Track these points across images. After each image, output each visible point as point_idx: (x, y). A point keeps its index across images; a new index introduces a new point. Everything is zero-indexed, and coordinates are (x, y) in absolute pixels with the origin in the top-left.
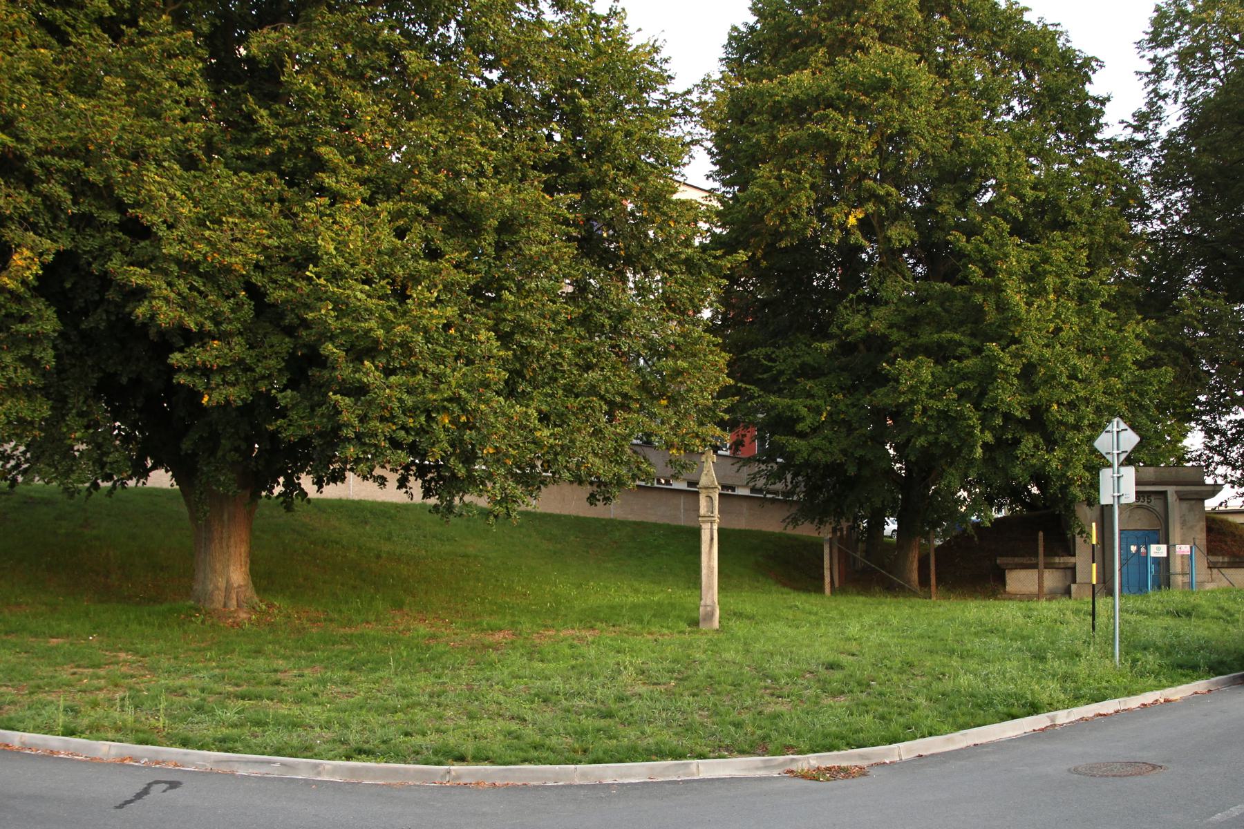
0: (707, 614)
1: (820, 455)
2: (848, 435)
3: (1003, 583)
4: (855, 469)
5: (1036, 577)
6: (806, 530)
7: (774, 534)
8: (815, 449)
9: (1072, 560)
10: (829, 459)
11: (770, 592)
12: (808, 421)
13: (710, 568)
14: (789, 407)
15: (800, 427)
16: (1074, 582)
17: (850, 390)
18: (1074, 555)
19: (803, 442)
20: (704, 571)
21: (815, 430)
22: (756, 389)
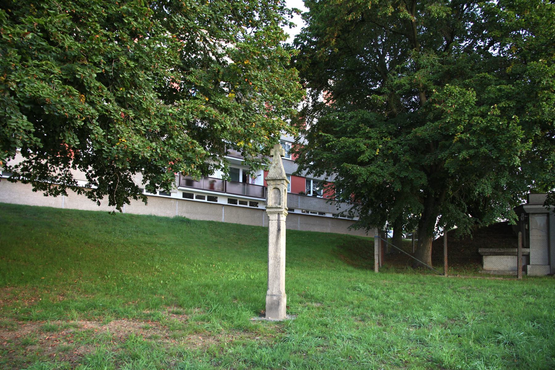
0: (272, 304)
1: (375, 177)
2: (394, 165)
3: (482, 264)
4: (400, 186)
5: (538, 264)
6: (360, 233)
7: (343, 235)
8: (372, 173)
9: (527, 250)
10: (379, 180)
11: (339, 271)
12: (367, 154)
13: (277, 258)
14: (354, 144)
15: (361, 158)
16: (529, 264)
17: (396, 135)
18: (529, 247)
19: (363, 169)
20: (271, 262)
21: (371, 161)
22: (331, 136)
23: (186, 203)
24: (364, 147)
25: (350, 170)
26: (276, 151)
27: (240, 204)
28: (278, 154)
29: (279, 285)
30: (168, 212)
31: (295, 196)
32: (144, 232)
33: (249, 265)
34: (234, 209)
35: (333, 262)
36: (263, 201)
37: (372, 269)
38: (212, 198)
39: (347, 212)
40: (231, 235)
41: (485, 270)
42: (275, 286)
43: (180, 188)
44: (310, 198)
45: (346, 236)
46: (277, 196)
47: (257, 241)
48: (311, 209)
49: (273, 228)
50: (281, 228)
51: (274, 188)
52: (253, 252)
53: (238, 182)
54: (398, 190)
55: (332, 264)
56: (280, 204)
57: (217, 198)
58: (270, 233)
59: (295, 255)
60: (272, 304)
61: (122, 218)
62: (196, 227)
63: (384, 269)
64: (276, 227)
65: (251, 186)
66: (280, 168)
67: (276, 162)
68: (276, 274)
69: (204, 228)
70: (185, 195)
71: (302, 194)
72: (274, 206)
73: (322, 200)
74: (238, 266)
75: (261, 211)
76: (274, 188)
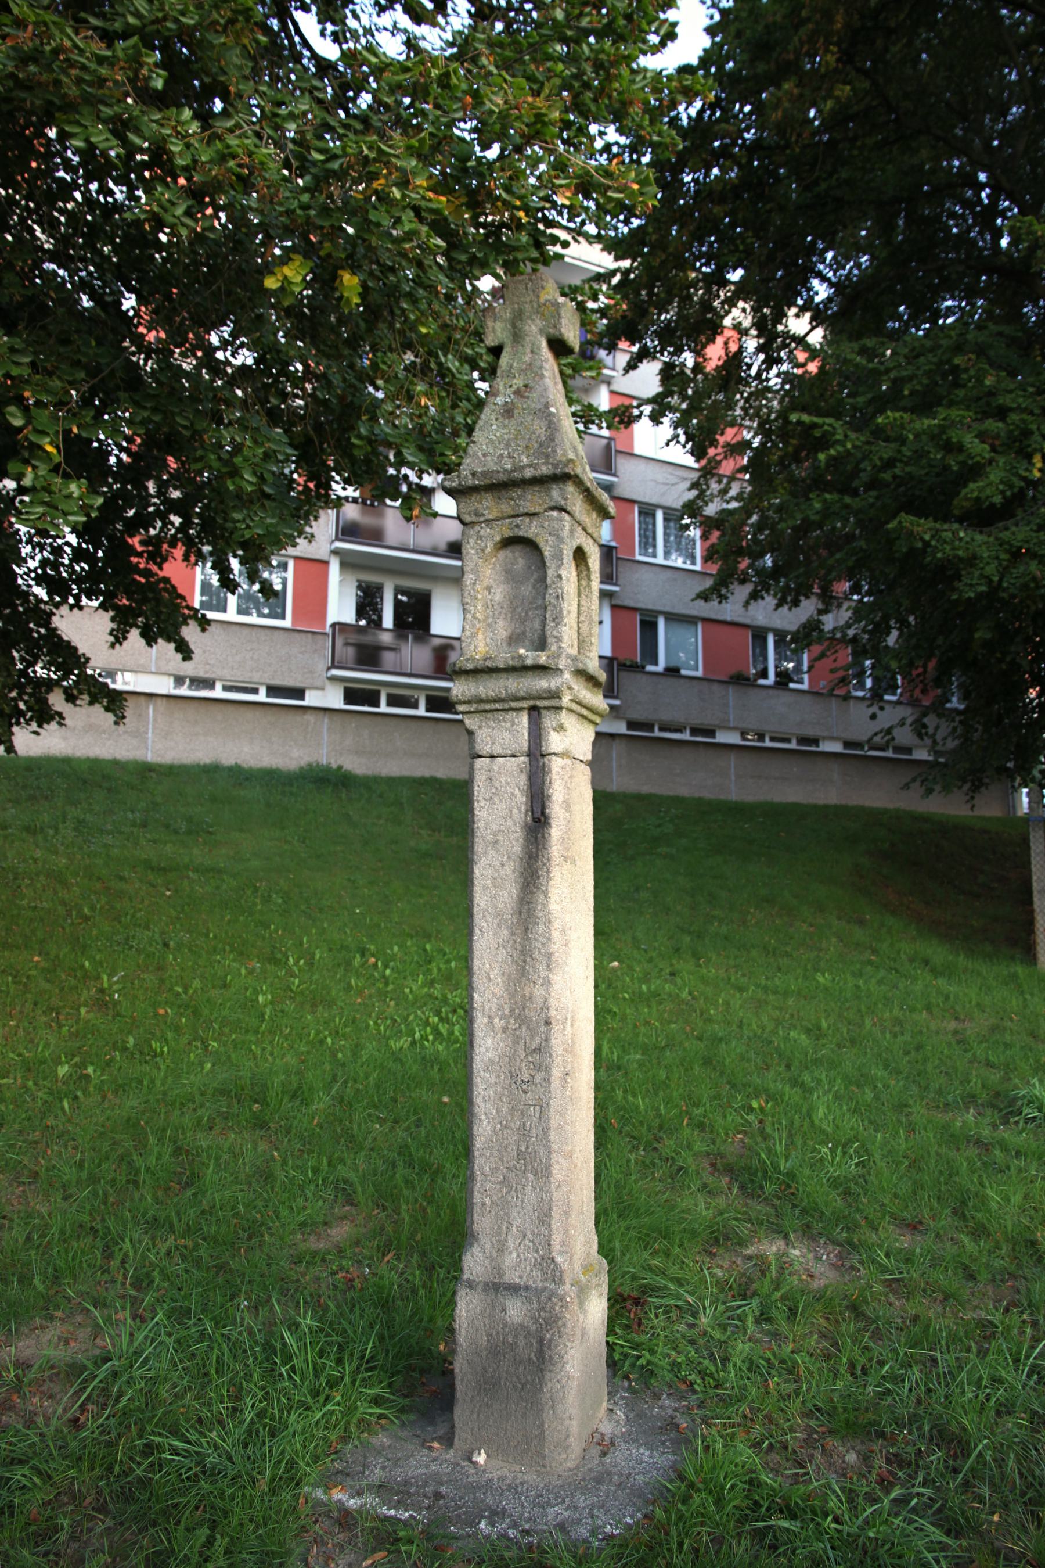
0: (498, 1348)
12: (995, 475)
13: (532, 1026)
19: (978, 537)
23: (353, 723)
24: (979, 449)
25: (927, 544)
28: (535, 331)
29: (544, 1217)
30: (296, 753)
31: (715, 687)
32: (167, 826)
35: (861, 923)
39: (907, 729)
42: (517, 1222)
43: (335, 672)
44: (764, 693)
45: (898, 816)
46: (527, 590)
49: (496, 812)
50: (556, 810)
55: (859, 934)
56: (541, 644)
58: (479, 846)
61: (106, 777)
66: (544, 413)
67: (518, 382)
68: (524, 1132)
70: (352, 695)
71: (740, 680)
72: (503, 658)
73: (808, 698)
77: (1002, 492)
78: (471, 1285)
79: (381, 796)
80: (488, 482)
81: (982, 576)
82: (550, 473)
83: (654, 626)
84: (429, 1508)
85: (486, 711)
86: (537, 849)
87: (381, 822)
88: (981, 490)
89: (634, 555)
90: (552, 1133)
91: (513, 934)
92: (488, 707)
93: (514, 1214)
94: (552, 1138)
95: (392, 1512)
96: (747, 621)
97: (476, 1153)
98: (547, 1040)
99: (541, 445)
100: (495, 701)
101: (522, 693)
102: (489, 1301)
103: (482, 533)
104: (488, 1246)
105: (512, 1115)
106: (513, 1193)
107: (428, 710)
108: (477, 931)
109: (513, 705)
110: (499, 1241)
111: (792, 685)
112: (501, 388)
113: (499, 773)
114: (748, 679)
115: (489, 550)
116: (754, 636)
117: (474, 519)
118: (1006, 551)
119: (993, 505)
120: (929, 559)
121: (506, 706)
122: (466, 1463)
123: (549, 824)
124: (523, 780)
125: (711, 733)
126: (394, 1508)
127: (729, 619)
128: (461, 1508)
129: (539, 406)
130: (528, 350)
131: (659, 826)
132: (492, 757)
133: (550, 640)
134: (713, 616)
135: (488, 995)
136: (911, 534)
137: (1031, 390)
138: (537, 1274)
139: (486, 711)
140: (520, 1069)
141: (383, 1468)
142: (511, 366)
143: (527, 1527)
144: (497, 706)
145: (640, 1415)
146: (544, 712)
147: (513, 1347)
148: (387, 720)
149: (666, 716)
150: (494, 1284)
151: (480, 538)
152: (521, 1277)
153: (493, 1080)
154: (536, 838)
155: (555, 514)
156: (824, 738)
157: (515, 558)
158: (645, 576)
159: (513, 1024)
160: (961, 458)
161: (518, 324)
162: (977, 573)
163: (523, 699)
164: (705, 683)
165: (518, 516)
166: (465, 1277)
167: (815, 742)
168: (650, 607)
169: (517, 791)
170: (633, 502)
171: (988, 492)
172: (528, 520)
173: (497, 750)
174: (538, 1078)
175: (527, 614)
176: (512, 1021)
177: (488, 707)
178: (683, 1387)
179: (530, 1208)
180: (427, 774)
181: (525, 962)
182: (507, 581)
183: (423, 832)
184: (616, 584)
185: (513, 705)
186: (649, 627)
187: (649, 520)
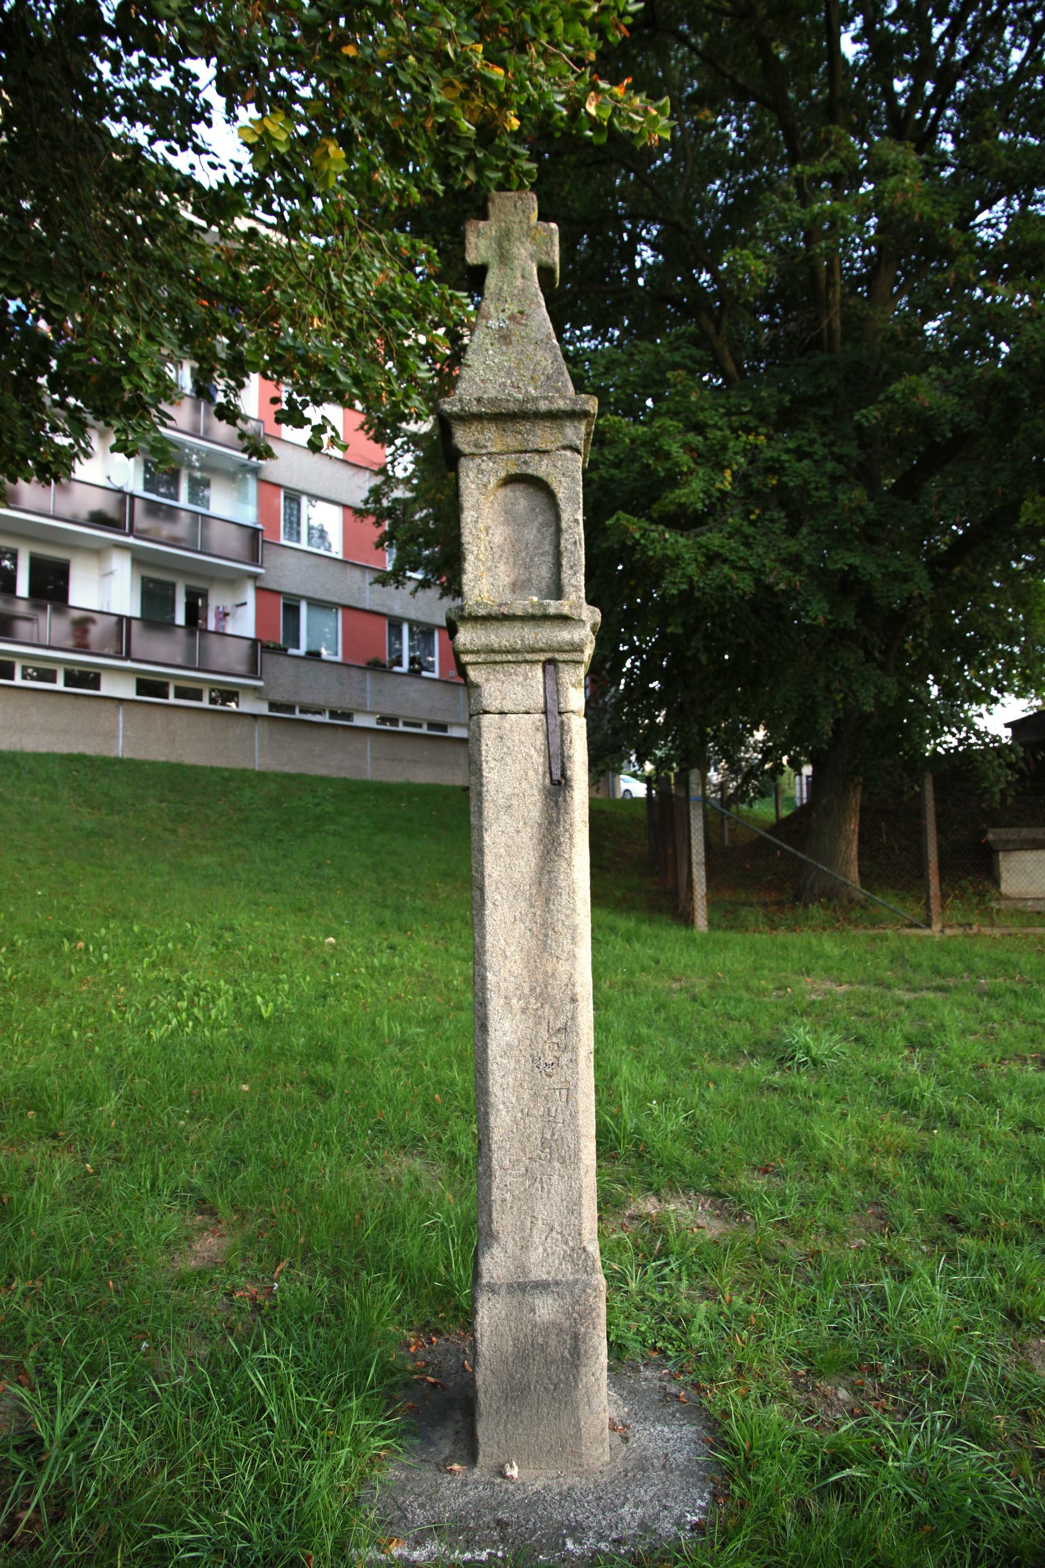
19: (682, 540)
25: (637, 542)
26: (504, 237)
27: (177, 696)
31: (354, 672)
33: (232, 929)
34: (158, 715)
36: (255, 689)
37: (687, 920)
38: (84, 678)
40: (152, 802)
41: (1008, 898)
42: (542, 1212)
44: (399, 679)
46: (531, 534)
47: (246, 821)
48: (404, 711)
51: (511, 480)
52: (239, 866)
53: (169, 625)
54: (821, 620)
57: (98, 677)
58: (489, 811)
59: (396, 874)
60: (523, 1355)
62: (19, 777)
63: (726, 916)
64: (538, 760)
65: (214, 641)
67: (512, 308)
68: (549, 1117)
69: (49, 779)
71: (376, 667)
74: (186, 940)
75: (247, 721)
76: (511, 480)
77: (703, 501)
78: (493, 1289)
79: (30, 772)
80: (495, 410)
81: (684, 575)
82: (569, 408)
83: (296, 610)
84: (503, 1539)
85: (496, 663)
86: (558, 814)
87: (36, 799)
88: (687, 496)
89: (279, 539)
90: (581, 1116)
91: (532, 906)
92: (498, 658)
93: (539, 1207)
94: (581, 1122)
95: (468, 1555)
96: (385, 610)
97: (494, 1147)
98: (573, 1018)
99: (548, 378)
100: (508, 652)
101: (541, 645)
102: (515, 1302)
103: (484, 466)
104: (510, 1245)
105: (535, 1102)
106: (538, 1185)
107: (66, 685)
108: (489, 904)
109: (529, 657)
110: (523, 1238)
111: (425, 674)
112: (492, 310)
113: (511, 731)
114: (384, 666)
115: (491, 486)
116: (390, 625)
117: (474, 450)
118: (704, 555)
119: (695, 510)
120: (638, 556)
121: (520, 658)
122: (499, 1480)
123: (571, 787)
124: (540, 737)
125: (348, 716)
126: (467, 1549)
127: (368, 607)
128: (535, 1531)
129: (539, 337)
130: (519, 275)
131: (318, 804)
132: (501, 713)
133: (568, 589)
134: (353, 604)
135: (504, 973)
136: (626, 531)
137: (722, 410)
138: (567, 1267)
139: (496, 663)
140: (543, 1051)
141: (422, 1506)
142: (501, 289)
143: (614, 1535)
144: (510, 657)
145: (633, 1392)
146: (561, 666)
147: (543, 1348)
148: (24, 693)
149: (306, 698)
150: (519, 1284)
151: (482, 472)
152: (548, 1273)
153: (513, 1064)
154: (557, 802)
155: (568, 453)
156: (453, 724)
157: (516, 498)
158: (290, 560)
159: (534, 1004)
160: (668, 465)
161: (505, 244)
162: (680, 572)
163: (542, 650)
164: (344, 668)
165: (526, 452)
166: (484, 1281)
167: (444, 727)
168: (294, 591)
169: (533, 752)
170: (279, 486)
171: (692, 498)
172: (537, 458)
173: (508, 706)
174: (564, 1061)
175: (532, 560)
176: (533, 1001)
177: (498, 658)
178: (655, 1355)
179: (558, 1199)
180: (75, 751)
181: (546, 935)
182: (507, 522)
183: (83, 810)
184: (261, 567)
185: (529, 657)
186: (292, 611)
187: (294, 506)
